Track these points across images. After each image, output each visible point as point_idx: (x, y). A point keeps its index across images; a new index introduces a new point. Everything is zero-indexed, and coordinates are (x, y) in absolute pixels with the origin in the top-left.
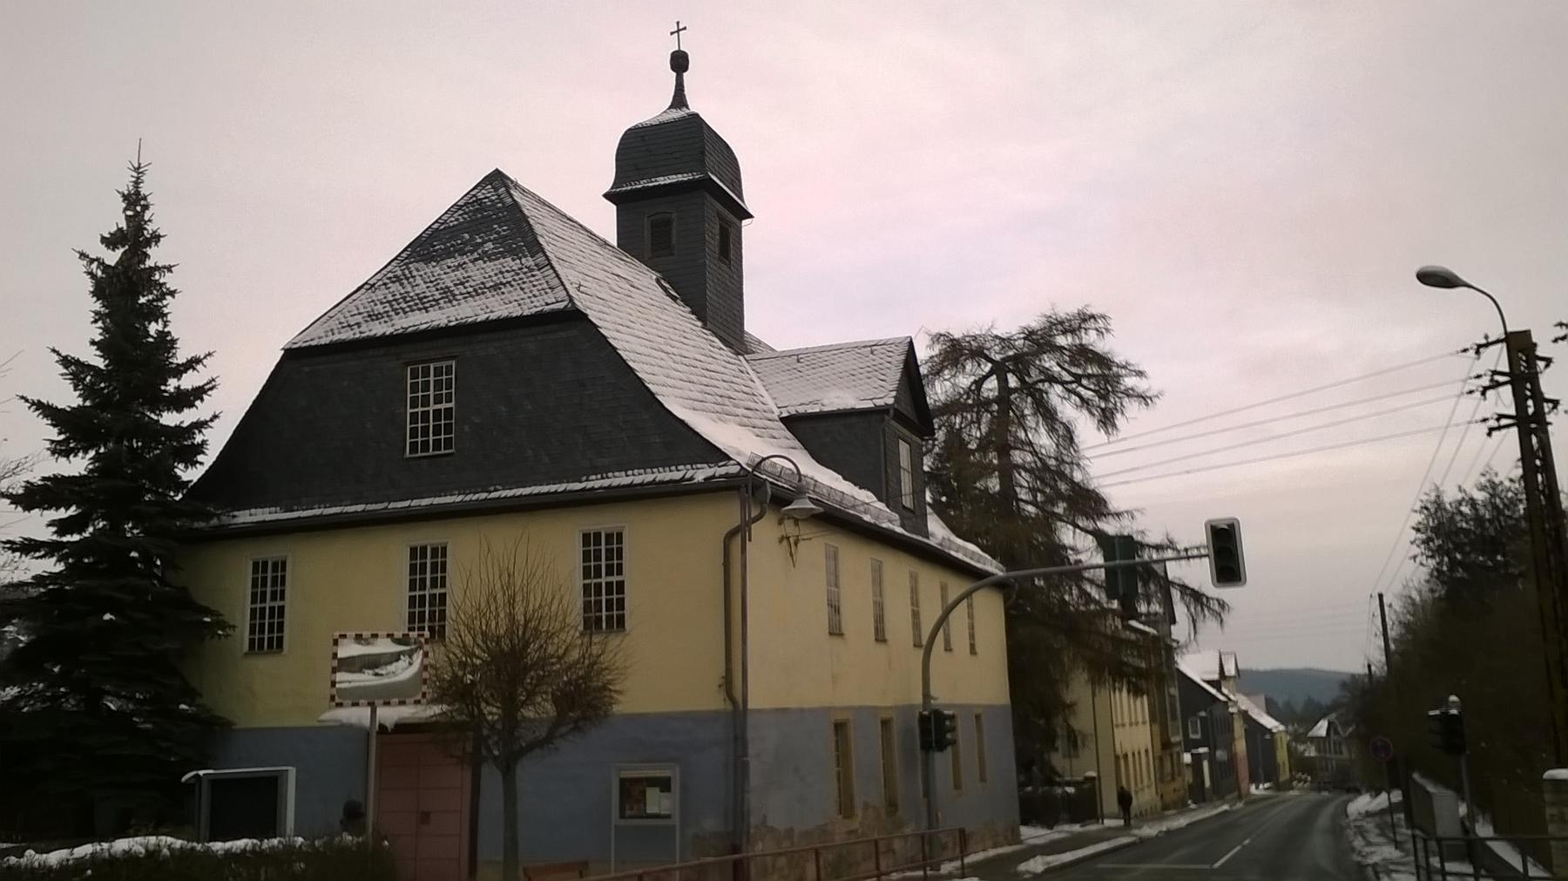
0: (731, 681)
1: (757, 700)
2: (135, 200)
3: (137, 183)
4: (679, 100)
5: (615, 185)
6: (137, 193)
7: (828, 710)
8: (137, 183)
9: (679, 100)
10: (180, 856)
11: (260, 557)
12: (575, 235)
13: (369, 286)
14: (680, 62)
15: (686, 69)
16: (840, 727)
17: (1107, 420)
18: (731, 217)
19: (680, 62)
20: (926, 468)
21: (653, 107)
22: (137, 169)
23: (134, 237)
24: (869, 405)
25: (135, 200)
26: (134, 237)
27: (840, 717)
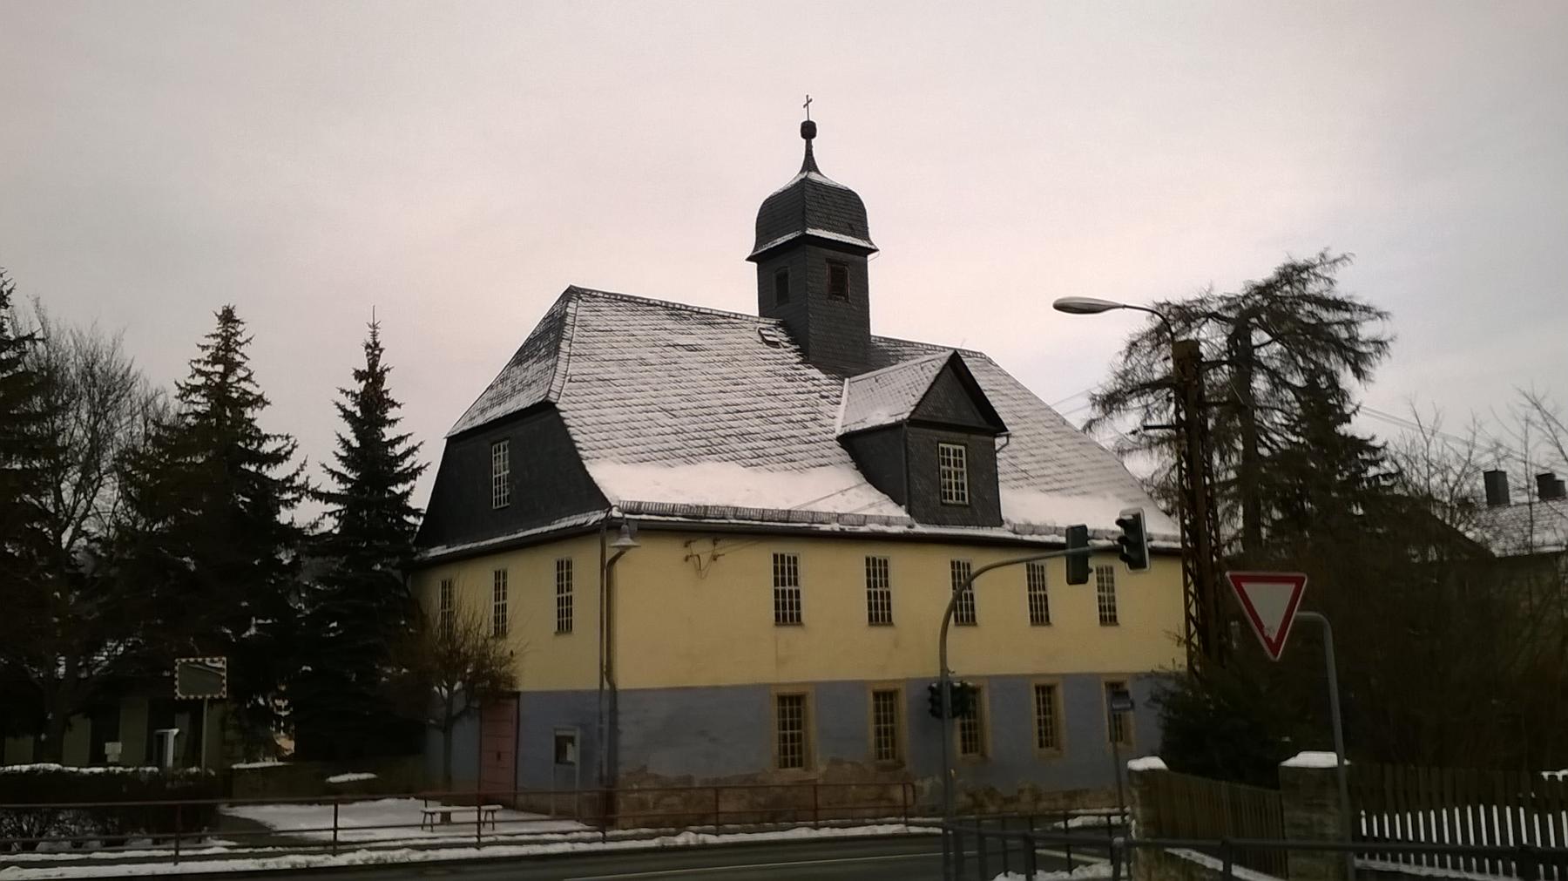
0: (607, 670)
1: (622, 683)
2: (374, 350)
3: (374, 335)
4: (809, 164)
5: (756, 249)
6: (376, 345)
7: (923, 680)
8: (374, 335)
9: (809, 164)
10: (58, 771)
11: (779, 552)
12: (649, 320)
13: (491, 387)
14: (809, 130)
15: (814, 136)
16: (1045, 691)
17: (1359, 373)
18: (857, 258)
19: (809, 130)
20: (286, 562)
21: (786, 174)
22: (374, 327)
23: (373, 377)
24: (892, 420)
25: (374, 350)
26: (373, 377)
27: (1046, 682)
